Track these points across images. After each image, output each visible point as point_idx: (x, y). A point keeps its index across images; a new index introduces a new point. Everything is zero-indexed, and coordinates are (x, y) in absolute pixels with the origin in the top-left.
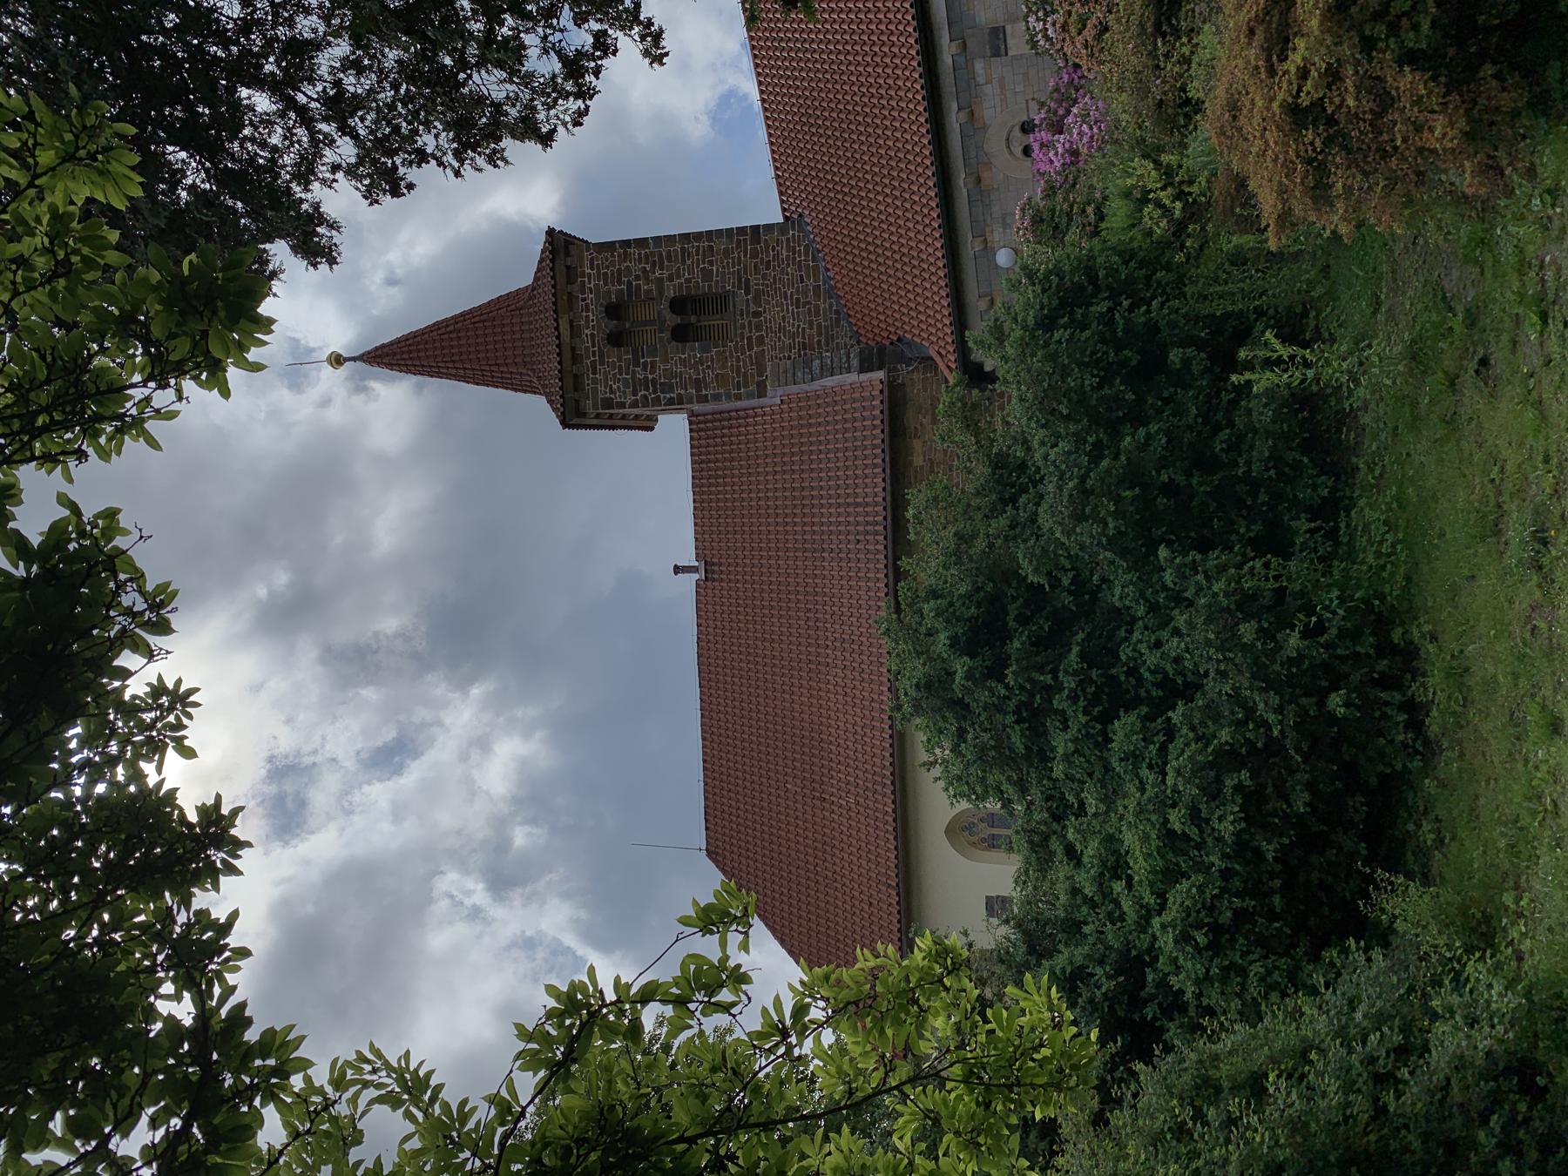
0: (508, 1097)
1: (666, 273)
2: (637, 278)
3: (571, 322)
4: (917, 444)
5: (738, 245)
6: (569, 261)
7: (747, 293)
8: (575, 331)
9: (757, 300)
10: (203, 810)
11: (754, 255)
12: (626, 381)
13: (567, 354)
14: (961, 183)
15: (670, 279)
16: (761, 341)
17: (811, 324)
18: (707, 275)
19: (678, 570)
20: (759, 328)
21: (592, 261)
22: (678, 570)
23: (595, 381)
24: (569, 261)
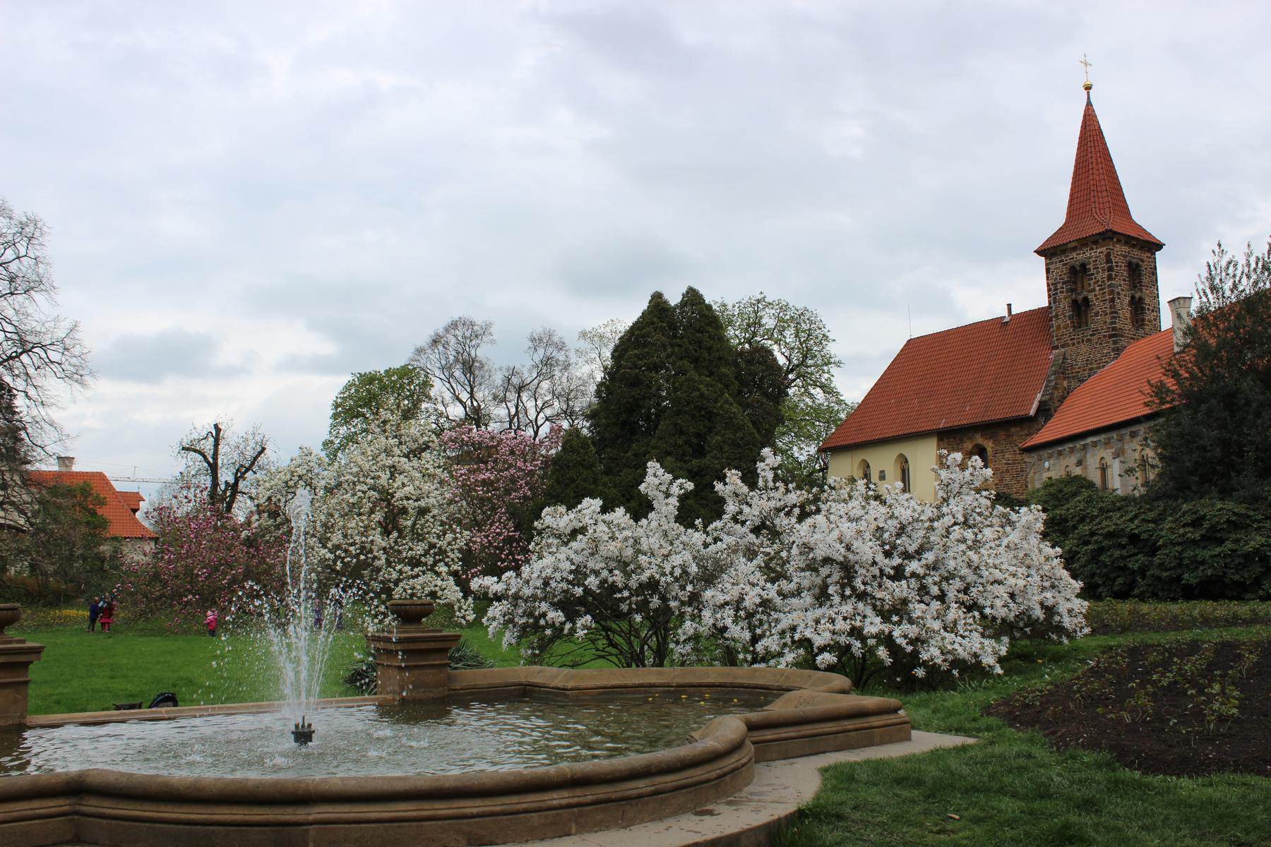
0: (705, 808)
1: (1097, 293)
2: (1095, 278)
3: (1076, 247)
4: (1018, 429)
5: (1108, 328)
6: (1100, 241)
7: (1091, 335)
8: (1074, 249)
9: (1089, 340)
10: (725, 476)
11: (1105, 336)
12: (1056, 279)
13: (1064, 248)
14: (269, 777)
15: (1095, 295)
16: (1074, 344)
17: (1079, 368)
18: (1097, 314)
19: (1009, 305)
20: (1078, 343)
21: (1102, 252)
22: (1009, 305)
23: (1056, 263)
24: (1100, 241)
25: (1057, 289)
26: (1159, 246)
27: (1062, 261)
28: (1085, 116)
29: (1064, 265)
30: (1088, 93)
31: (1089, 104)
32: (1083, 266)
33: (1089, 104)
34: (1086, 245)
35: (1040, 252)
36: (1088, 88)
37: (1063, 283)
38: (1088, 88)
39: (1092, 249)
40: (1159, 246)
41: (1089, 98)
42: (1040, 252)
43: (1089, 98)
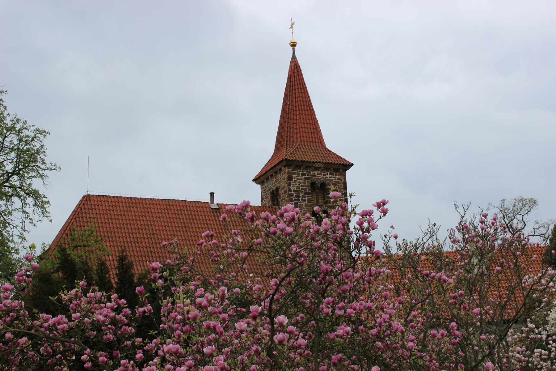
3: (320, 168)
8: (316, 169)
12: (298, 188)
19: (212, 194)
22: (212, 194)
23: (298, 174)
25: (300, 197)
26: (349, 166)
27: (304, 174)
28: (290, 77)
29: (305, 178)
30: (294, 49)
31: (294, 57)
32: (323, 185)
33: (294, 57)
34: (327, 169)
35: (253, 181)
36: (293, 45)
37: (305, 193)
38: (293, 45)
39: (331, 174)
40: (349, 166)
41: (294, 53)
42: (253, 181)
43: (294, 53)
